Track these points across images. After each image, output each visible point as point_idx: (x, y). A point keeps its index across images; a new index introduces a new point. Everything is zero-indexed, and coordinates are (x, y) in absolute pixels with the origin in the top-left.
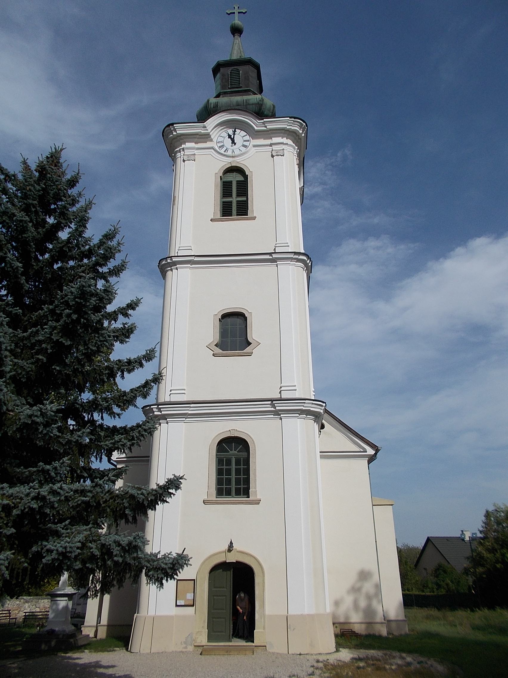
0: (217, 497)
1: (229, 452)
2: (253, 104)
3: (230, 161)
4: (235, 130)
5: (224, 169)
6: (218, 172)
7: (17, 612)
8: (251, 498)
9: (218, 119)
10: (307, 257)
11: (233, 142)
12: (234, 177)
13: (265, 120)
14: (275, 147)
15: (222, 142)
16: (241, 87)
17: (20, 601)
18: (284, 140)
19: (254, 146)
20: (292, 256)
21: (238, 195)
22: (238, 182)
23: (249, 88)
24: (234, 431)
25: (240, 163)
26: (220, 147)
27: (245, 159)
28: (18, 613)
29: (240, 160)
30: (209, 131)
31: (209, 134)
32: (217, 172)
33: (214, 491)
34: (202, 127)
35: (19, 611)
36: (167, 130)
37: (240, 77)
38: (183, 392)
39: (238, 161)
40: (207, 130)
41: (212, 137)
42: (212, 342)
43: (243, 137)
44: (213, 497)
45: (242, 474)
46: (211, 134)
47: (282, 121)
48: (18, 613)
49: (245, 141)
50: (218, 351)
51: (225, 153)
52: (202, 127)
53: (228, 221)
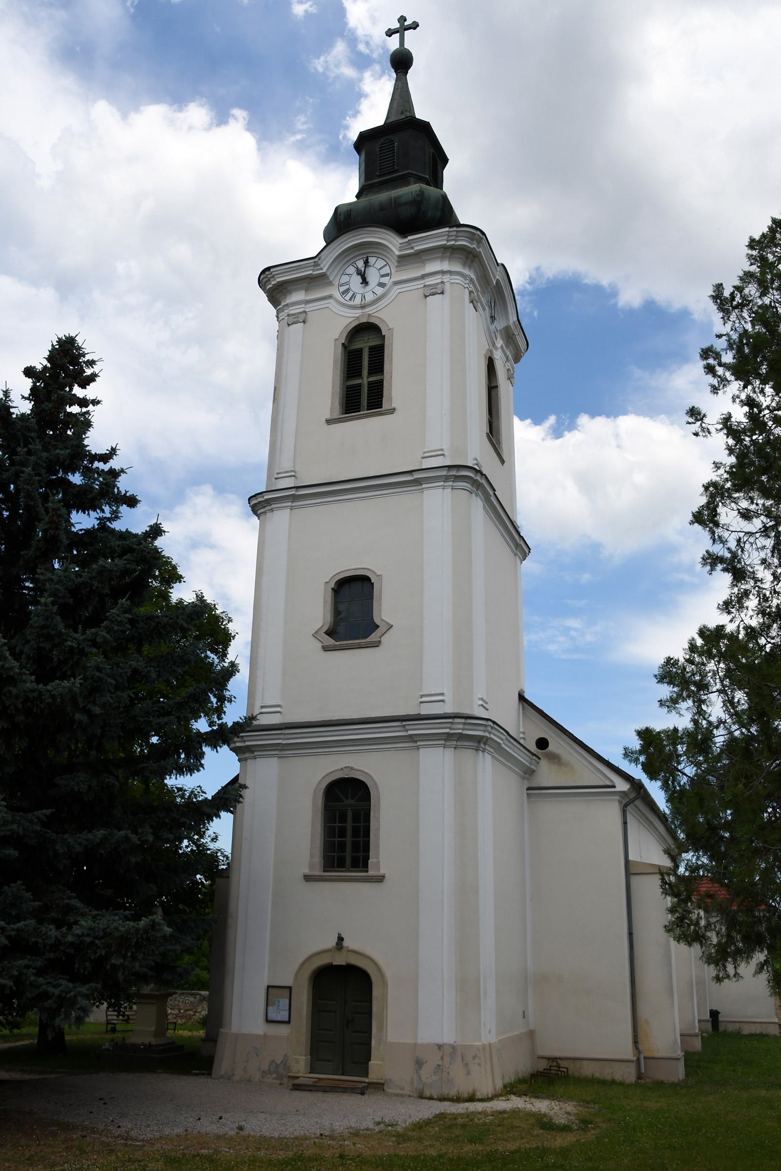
0: (326, 869)
1: (344, 801)
2: (406, 203)
3: (358, 315)
4: (367, 260)
5: (349, 330)
6: (339, 336)
7: (191, 1013)
8: (371, 872)
9: (340, 246)
10: (472, 470)
11: (365, 282)
12: (366, 340)
13: (410, 238)
14: (430, 281)
15: (347, 283)
16: (396, 171)
17: (195, 998)
18: (445, 266)
19: (396, 283)
20: (444, 473)
21: (370, 373)
22: (371, 349)
23: (408, 171)
24: (347, 769)
25: (374, 316)
26: (343, 293)
27: (378, 309)
28: (193, 1015)
29: (375, 311)
30: (324, 270)
31: (326, 275)
32: (337, 338)
33: (318, 859)
34: (312, 266)
35: (195, 1012)
36: (263, 279)
37: (394, 152)
38: (278, 709)
39: (370, 313)
40: (322, 269)
41: (331, 278)
42: (321, 627)
43: (380, 269)
44: (318, 872)
45: (362, 834)
46: (328, 274)
47: (435, 236)
48: (193, 1015)
49: (383, 276)
50: (330, 641)
51: (351, 303)
52: (312, 266)
53: (351, 420)
